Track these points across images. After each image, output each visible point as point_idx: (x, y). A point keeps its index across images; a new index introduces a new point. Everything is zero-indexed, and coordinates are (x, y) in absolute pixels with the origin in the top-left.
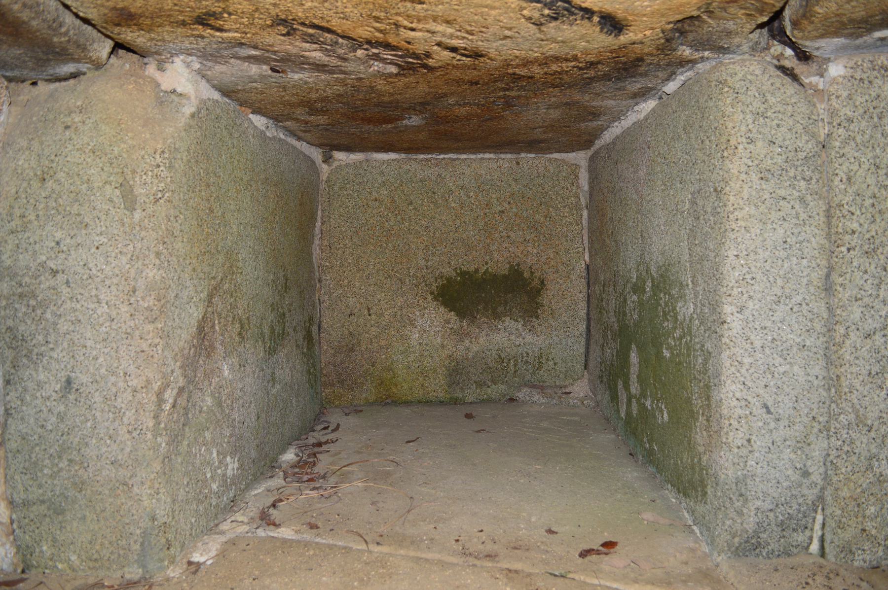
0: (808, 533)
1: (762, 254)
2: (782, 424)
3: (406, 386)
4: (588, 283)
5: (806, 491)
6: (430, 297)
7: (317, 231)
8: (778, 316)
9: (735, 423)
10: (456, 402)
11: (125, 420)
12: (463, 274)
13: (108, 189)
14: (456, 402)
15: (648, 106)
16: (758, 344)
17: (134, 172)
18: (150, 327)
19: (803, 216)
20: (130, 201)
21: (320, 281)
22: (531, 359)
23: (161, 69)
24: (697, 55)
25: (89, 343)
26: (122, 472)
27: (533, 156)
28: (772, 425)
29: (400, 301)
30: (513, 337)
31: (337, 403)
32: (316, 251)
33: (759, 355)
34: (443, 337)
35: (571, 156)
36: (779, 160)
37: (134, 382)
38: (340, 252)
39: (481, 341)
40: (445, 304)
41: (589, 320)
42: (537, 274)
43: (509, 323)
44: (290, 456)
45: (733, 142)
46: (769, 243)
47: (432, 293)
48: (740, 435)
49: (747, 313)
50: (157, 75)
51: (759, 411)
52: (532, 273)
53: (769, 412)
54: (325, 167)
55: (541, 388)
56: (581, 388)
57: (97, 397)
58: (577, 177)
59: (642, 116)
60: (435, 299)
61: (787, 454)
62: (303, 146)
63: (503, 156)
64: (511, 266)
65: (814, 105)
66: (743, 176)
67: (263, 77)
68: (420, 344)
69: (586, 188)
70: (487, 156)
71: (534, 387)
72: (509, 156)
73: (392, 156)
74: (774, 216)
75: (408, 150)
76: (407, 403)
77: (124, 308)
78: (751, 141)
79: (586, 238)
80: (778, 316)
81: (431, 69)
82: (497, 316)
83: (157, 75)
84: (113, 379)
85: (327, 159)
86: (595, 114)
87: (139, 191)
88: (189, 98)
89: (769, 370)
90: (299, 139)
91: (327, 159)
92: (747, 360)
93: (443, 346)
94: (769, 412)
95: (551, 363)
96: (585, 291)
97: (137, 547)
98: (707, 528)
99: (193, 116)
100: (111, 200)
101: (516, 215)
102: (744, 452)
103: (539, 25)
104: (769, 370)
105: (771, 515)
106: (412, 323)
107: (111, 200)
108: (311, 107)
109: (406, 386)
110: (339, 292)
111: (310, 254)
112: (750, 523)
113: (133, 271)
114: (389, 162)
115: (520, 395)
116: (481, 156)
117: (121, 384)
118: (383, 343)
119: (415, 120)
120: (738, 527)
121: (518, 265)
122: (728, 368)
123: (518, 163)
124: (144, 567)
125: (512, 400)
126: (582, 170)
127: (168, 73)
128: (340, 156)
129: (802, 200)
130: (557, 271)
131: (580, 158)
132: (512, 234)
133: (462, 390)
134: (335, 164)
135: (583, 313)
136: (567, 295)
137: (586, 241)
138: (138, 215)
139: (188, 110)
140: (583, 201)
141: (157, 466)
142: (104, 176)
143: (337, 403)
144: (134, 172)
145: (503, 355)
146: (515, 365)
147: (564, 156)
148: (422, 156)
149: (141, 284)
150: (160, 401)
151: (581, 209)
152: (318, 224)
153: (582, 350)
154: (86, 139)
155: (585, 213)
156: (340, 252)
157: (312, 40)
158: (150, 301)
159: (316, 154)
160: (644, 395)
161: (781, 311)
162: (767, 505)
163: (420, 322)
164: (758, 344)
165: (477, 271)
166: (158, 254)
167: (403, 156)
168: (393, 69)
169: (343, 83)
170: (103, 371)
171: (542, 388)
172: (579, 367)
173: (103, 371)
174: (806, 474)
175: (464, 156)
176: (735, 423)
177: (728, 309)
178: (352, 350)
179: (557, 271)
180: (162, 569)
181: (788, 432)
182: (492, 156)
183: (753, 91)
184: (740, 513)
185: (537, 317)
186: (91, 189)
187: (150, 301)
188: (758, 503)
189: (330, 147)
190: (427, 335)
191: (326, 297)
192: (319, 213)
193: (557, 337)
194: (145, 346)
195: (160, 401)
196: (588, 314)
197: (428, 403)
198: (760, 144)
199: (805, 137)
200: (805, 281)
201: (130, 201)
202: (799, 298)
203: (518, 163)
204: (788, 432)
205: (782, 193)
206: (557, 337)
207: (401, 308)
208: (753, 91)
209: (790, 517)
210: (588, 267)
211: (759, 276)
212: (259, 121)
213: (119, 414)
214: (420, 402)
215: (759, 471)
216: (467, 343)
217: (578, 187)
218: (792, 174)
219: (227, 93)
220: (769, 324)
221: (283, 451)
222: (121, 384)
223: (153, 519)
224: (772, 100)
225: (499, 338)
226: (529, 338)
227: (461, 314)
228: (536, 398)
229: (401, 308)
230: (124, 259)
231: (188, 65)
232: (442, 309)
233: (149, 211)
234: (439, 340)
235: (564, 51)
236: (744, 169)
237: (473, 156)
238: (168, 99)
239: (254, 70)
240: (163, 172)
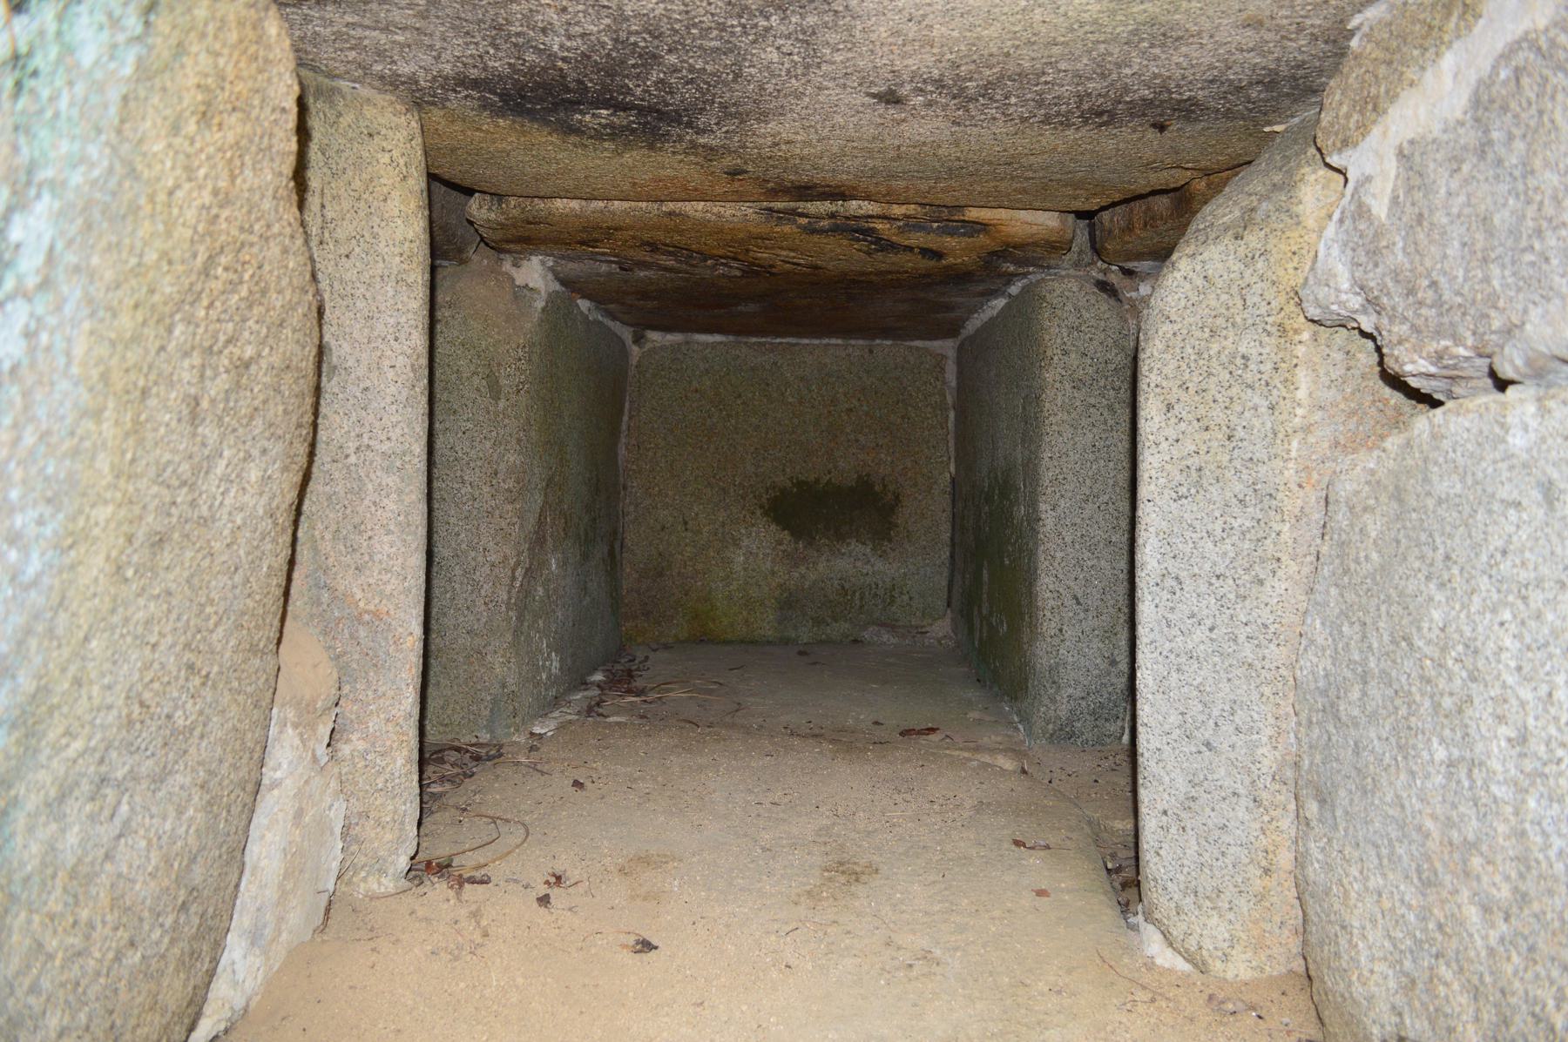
0: (1119, 723)
1: (1073, 457)
2: (1090, 615)
3: (725, 622)
4: (953, 501)
5: (1114, 680)
6: (758, 512)
7: (624, 427)
8: (1087, 514)
9: (1048, 614)
10: (785, 642)
11: (483, 593)
12: (800, 484)
13: (476, 381)
14: (785, 642)
15: (999, 303)
16: (1068, 539)
17: (499, 364)
18: (510, 507)
19: (1110, 422)
20: (495, 391)
21: (625, 488)
22: (881, 592)
23: (516, 265)
24: (1021, 270)
25: (452, 520)
26: (477, 641)
27: (889, 342)
28: (1082, 615)
29: (722, 516)
30: (859, 564)
31: (640, 640)
32: (622, 451)
33: (1070, 550)
34: (773, 561)
35: (936, 345)
36: (1090, 370)
37: (493, 558)
38: (650, 454)
39: (821, 567)
40: (777, 520)
41: (953, 545)
42: (891, 488)
43: (855, 547)
44: (598, 677)
45: (1049, 353)
46: (1079, 446)
47: (761, 507)
48: (1053, 625)
49: (1059, 510)
50: (513, 272)
51: (1070, 602)
52: (885, 486)
53: (1078, 603)
54: (635, 349)
55: (891, 626)
56: (941, 628)
57: (458, 571)
58: (943, 370)
59: (995, 313)
60: (766, 514)
61: (1096, 644)
62: (616, 326)
63: (853, 342)
64: (860, 477)
65: (1126, 321)
66: (1058, 385)
67: (610, 274)
68: (745, 569)
69: (954, 384)
70: (833, 341)
71: (883, 625)
72: (861, 342)
73: (718, 338)
74: (1084, 422)
75: (738, 333)
76: (726, 642)
77: (486, 489)
78: (1065, 353)
79: (952, 444)
80: (1087, 514)
81: (772, 274)
82: (841, 538)
83: (513, 272)
84: (473, 554)
85: (638, 339)
86: (949, 308)
87: (503, 382)
88: (539, 293)
89: (1079, 563)
90: (614, 318)
91: (638, 339)
92: (1059, 555)
93: (773, 573)
94: (1078, 603)
95: (906, 598)
96: (949, 509)
97: (487, 713)
98: (1025, 719)
99: (543, 310)
100: (478, 390)
101: (867, 414)
102: (1056, 641)
103: (869, 254)
104: (1079, 563)
105: (1084, 704)
106: (736, 543)
107: (478, 390)
108: (644, 295)
109: (725, 622)
110: (648, 502)
111: (616, 455)
112: (1063, 712)
113: (495, 456)
114: (714, 346)
115: (866, 635)
116: (826, 341)
117: (480, 559)
118: (699, 567)
119: (752, 307)
120: (1052, 713)
121: (868, 475)
122: (1043, 563)
123: (871, 352)
124: (492, 732)
125: (855, 641)
126: (950, 362)
127: (523, 270)
128: (654, 336)
129: (1110, 408)
130: (916, 485)
131: (947, 347)
132: (862, 438)
133: (795, 628)
134: (648, 346)
135: (946, 536)
136: (929, 515)
137: (952, 449)
138: (502, 404)
139: (540, 304)
140: (950, 400)
141: (509, 637)
142: (472, 368)
143: (640, 640)
144: (499, 364)
145: (847, 586)
146: (861, 599)
147: (928, 344)
148: (754, 340)
149: (502, 466)
150: (513, 578)
151: (947, 410)
152: (625, 418)
153: (944, 583)
154: (456, 333)
155: (952, 415)
156: (650, 454)
157: (671, 254)
158: (510, 484)
159: (626, 334)
160: (991, 613)
161: (1090, 509)
162: (1079, 693)
163: (746, 542)
164: (1068, 539)
165: (817, 481)
166: (519, 441)
167: (731, 338)
168: (738, 273)
169: (687, 280)
170: (464, 546)
171: (893, 628)
172: (941, 604)
173: (464, 546)
174: (1113, 663)
175: (806, 341)
176: (1048, 614)
177: (1043, 507)
178: (661, 575)
179: (916, 485)
180: (509, 735)
181: (1096, 622)
182: (840, 341)
183: (1069, 307)
184: (1053, 700)
185: (890, 541)
186: (460, 378)
187: (510, 484)
188: (1070, 691)
189: (642, 325)
190: (753, 559)
191: (632, 508)
192: (627, 405)
193: (915, 567)
194: (503, 525)
195: (513, 578)
196: (952, 539)
197: (753, 642)
198: (1073, 356)
199: (1114, 351)
200: (1111, 482)
201: (495, 391)
202: (1106, 498)
203: (871, 352)
204: (1096, 622)
205: (1092, 401)
206: (910, 569)
207: (723, 524)
208: (1069, 307)
209: (1102, 706)
210: (953, 480)
211: (1070, 477)
212: (584, 305)
213: (477, 587)
214: (742, 642)
215: (1070, 659)
216: (803, 570)
217: (944, 383)
218: (1102, 383)
219: (563, 282)
220: (1078, 521)
221: (591, 673)
222: (480, 559)
223: (504, 686)
224: (1086, 315)
225: (843, 565)
226: (880, 566)
227: (797, 534)
228: (885, 637)
229: (723, 524)
230: (488, 444)
231: (543, 263)
232: (773, 527)
233: (513, 401)
234: (769, 565)
235: (894, 268)
236: (1058, 378)
237: (816, 342)
238: (522, 293)
239: (604, 268)
240: (523, 365)
